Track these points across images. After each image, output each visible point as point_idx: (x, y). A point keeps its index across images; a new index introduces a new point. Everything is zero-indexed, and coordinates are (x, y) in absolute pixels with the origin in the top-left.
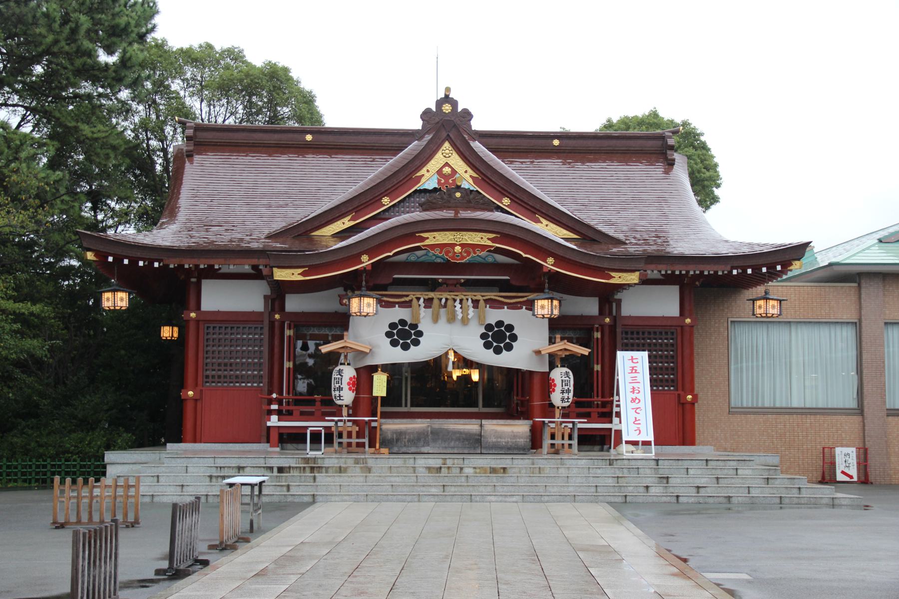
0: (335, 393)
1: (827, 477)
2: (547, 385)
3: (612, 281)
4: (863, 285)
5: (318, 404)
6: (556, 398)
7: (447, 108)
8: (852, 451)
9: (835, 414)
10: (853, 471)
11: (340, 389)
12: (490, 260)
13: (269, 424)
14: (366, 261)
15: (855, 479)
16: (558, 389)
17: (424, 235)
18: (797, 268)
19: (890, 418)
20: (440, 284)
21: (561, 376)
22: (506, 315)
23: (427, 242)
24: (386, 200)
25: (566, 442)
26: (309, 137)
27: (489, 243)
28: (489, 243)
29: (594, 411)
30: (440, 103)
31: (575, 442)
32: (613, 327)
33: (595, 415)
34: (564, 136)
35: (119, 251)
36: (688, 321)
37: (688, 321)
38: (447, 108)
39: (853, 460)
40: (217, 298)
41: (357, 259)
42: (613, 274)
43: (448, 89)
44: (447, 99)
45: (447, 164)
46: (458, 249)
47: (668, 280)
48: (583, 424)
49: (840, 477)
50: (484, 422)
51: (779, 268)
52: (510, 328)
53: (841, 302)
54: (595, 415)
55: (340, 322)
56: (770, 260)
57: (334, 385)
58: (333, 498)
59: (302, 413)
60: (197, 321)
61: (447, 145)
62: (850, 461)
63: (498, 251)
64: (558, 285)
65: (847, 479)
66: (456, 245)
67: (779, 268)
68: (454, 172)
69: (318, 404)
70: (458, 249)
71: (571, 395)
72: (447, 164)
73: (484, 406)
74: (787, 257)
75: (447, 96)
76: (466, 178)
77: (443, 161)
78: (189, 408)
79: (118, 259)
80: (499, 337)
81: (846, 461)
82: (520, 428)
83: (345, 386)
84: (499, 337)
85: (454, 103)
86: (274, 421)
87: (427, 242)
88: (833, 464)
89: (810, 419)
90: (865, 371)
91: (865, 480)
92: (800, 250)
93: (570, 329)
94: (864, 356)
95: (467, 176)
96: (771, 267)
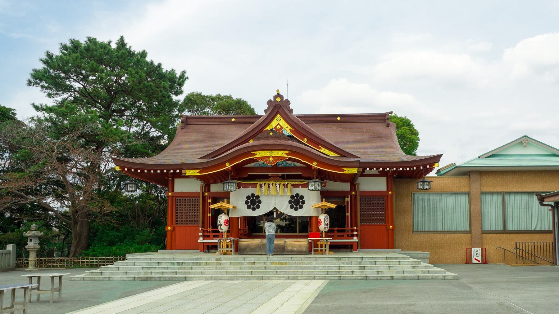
0: (219, 227)
1: (468, 260)
2: (318, 222)
3: (344, 172)
4: (471, 176)
5: (336, 232)
6: (322, 227)
7: (278, 99)
8: (479, 249)
9: (459, 233)
10: (480, 258)
11: (221, 225)
12: (293, 165)
13: (199, 241)
14: (228, 166)
15: (481, 262)
16: (323, 224)
17: (255, 153)
18: (437, 168)
19: (483, 235)
20: (270, 177)
21: (323, 218)
22: (301, 191)
23: (256, 156)
24: (251, 141)
25: (324, 248)
26: (233, 120)
27: (286, 156)
28: (286, 156)
29: (345, 234)
30: (275, 97)
31: (327, 249)
32: (356, 196)
33: (211, 236)
34: (342, 116)
35: (130, 166)
36: (390, 193)
37: (390, 193)
38: (278, 99)
39: (480, 254)
40: (181, 187)
41: (223, 164)
42: (345, 169)
43: (278, 91)
44: (279, 95)
45: (278, 124)
46: (271, 159)
47: (381, 174)
48: (331, 240)
49: (474, 261)
50: (286, 240)
51: (428, 167)
52: (302, 197)
53: (462, 185)
54: (346, 236)
55: (226, 196)
56: (425, 163)
57: (219, 223)
58: (195, 279)
59: (338, 236)
60: (172, 197)
61: (278, 115)
62: (478, 254)
63: (290, 159)
64: (322, 176)
65: (477, 262)
66: (270, 157)
67: (428, 167)
68: (282, 128)
69: (336, 232)
70: (271, 159)
71: (329, 226)
72: (278, 124)
73: (300, 232)
74: (432, 162)
75: (278, 94)
76: (287, 130)
77: (277, 122)
78: (169, 234)
79: (142, 171)
80: (297, 202)
81: (477, 253)
82: (303, 243)
83: (223, 224)
84: (297, 202)
85: (282, 97)
86: (201, 240)
87: (256, 156)
88: (471, 255)
89: (448, 236)
90: (472, 215)
91: (485, 262)
92: (437, 158)
93: (337, 197)
94: (472, 208)
95: (288, 129)
96: (425, 166)
